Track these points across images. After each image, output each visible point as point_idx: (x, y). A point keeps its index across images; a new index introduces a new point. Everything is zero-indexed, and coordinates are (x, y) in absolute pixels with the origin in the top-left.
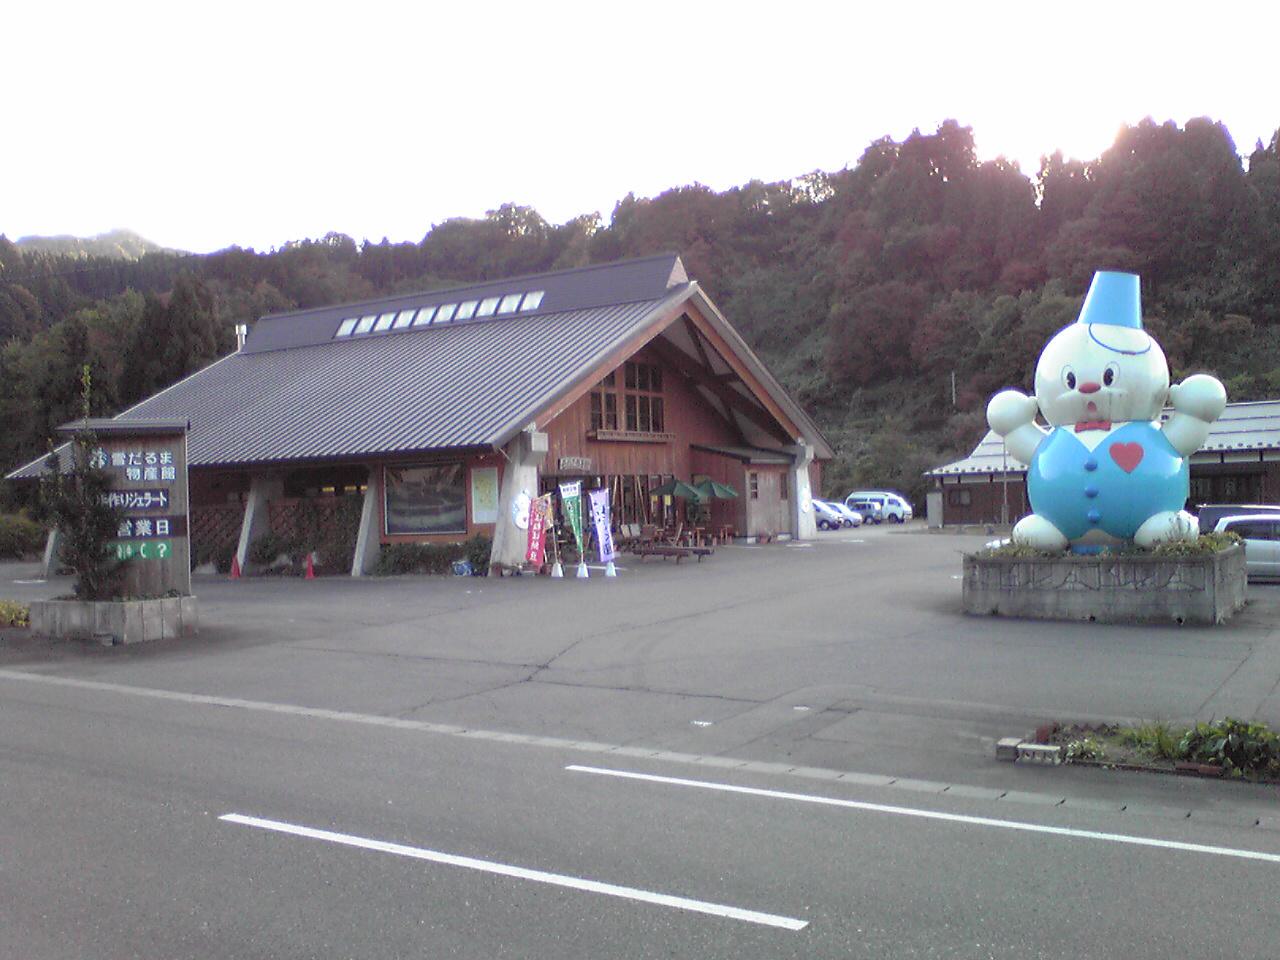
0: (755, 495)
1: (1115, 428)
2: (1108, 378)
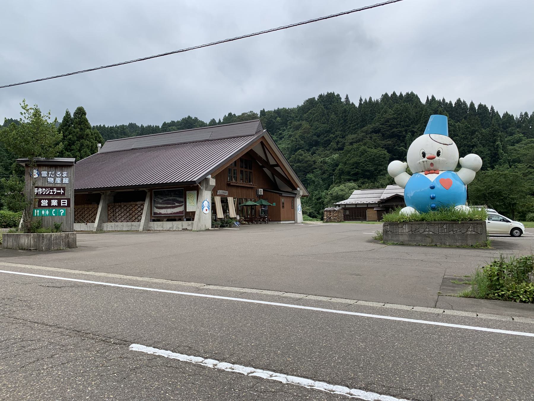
0: (283, 207)
1: (441, 173)
2: (438, 154)
